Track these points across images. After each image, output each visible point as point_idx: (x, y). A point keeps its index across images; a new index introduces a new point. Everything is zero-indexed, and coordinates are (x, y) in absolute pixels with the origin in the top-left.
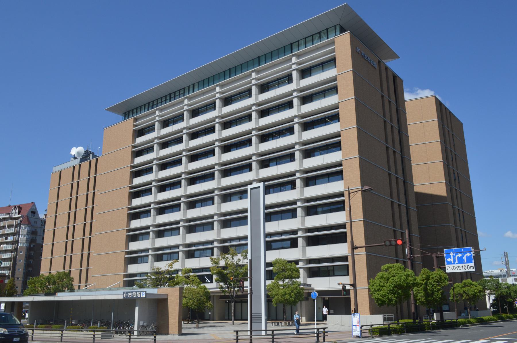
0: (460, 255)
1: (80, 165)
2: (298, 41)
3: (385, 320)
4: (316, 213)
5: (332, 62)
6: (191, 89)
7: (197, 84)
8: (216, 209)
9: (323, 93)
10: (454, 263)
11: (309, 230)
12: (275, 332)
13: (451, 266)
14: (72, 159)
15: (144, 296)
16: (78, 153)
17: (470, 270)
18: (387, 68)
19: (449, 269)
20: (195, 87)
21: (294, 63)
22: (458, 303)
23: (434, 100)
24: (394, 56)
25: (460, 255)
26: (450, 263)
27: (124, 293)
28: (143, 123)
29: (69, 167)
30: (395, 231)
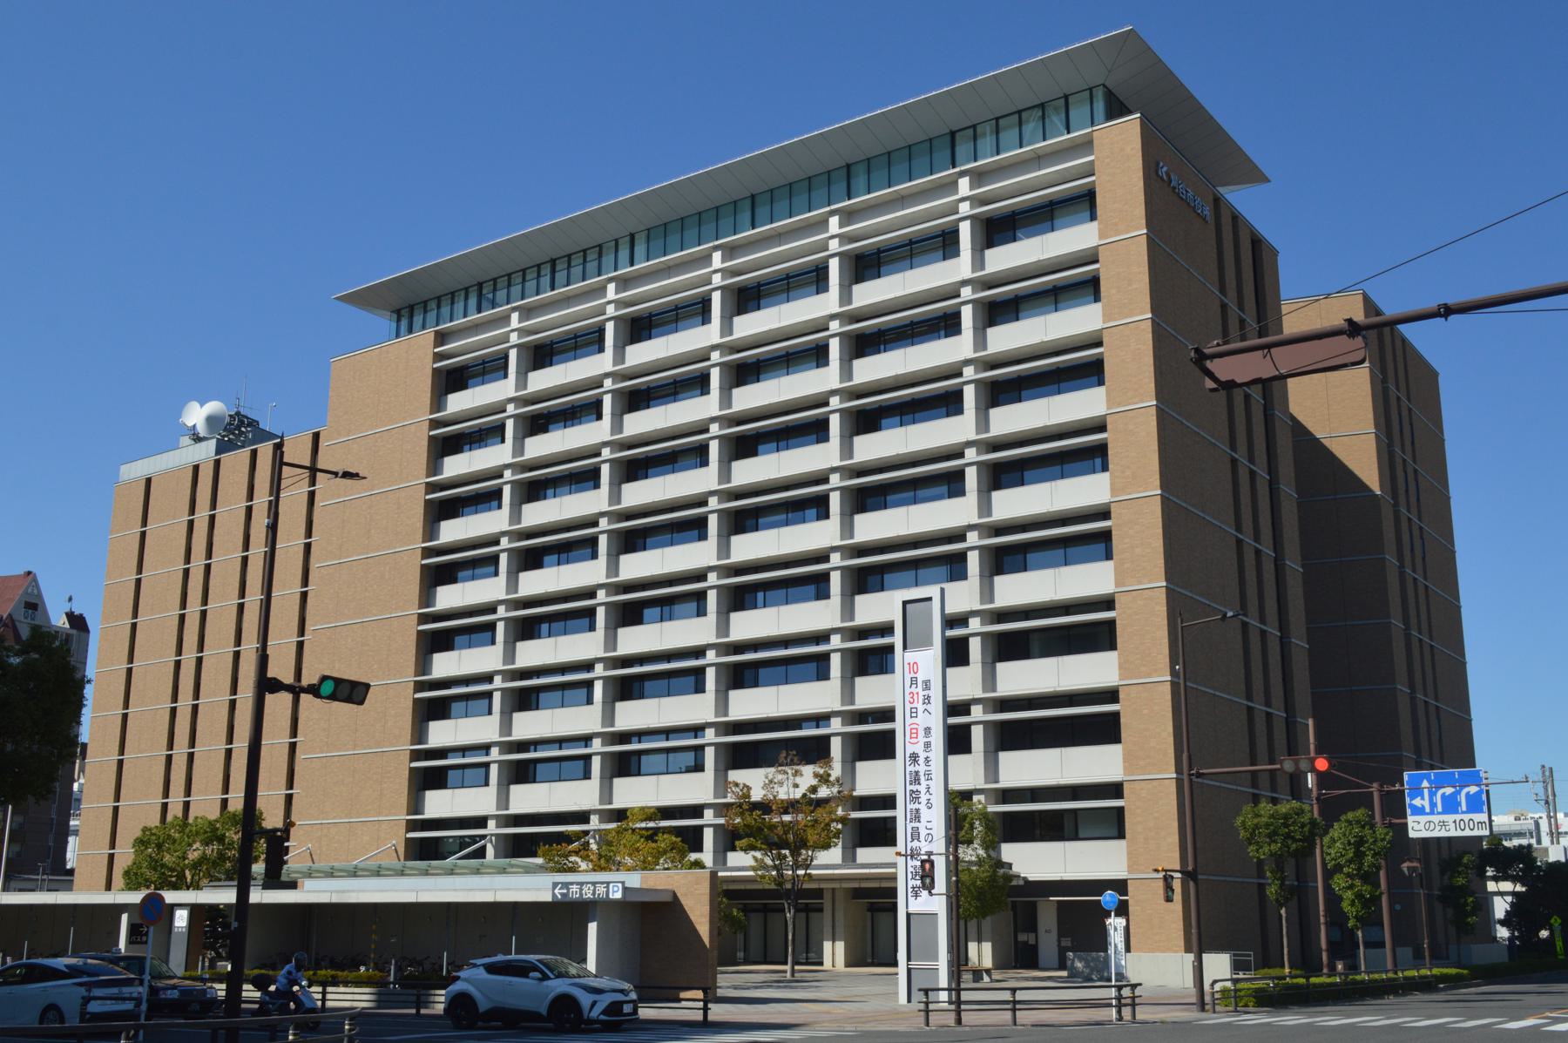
0: (1449, 791)
1: (217, 463)
2: (974, 127)
3: (1237, 966)
4: (1026, 655)
5: (1084, 203)
6: (624, 254)
7: (644, 235)
9: (1057, 296)
10: (1432, 813)
11: (1005, 704)
12: (1020, 996)
13: (1423, 819)
14: (186, 440)
15: (618, 895)
16: (211, 420)
17: (1476, 833)
18: (1236, 218)
19: (1417, 827)
20: (637, 249)
21: (963, 199)
22: (1442, 916)
23: (1361, 305)
24: (1252, 174)
25: (1449, 791)
26: (1419, 811)
27: (555, 885)
28: (466, 348)
29: (180, 469)
30: (1250, 709)
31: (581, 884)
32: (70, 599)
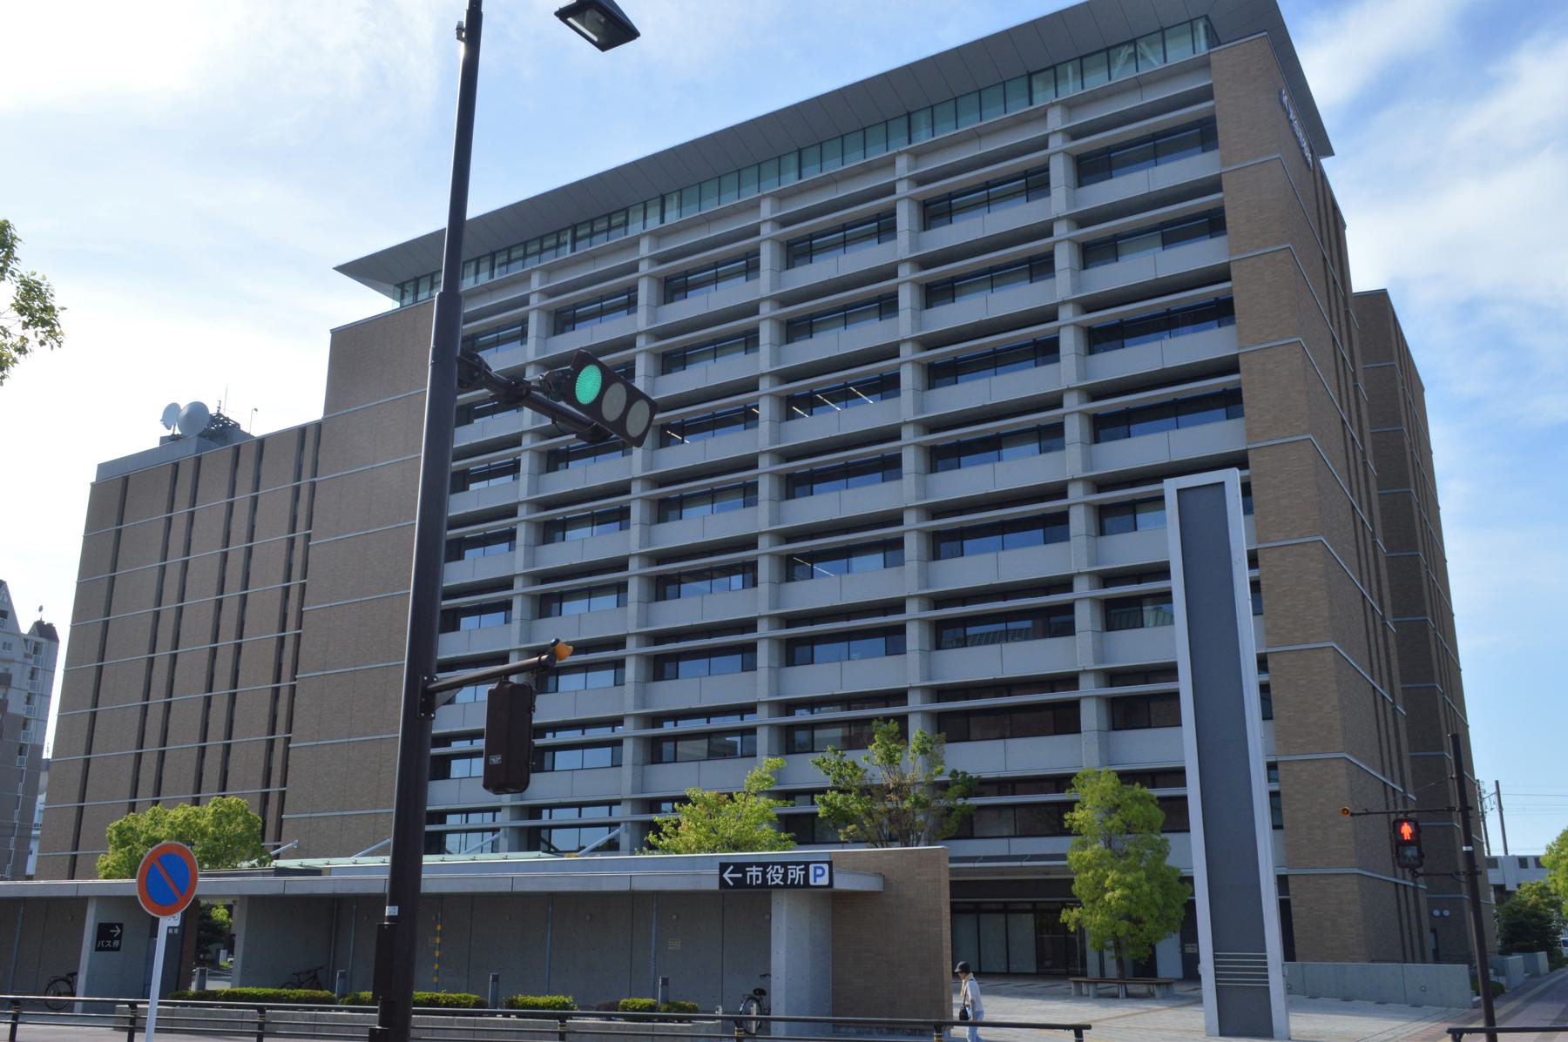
2: (1054, 67)
8: (1085, 559)
20: (668, 206)
27: (723, 867)
31: (765, 865)
32: (41, 609)
